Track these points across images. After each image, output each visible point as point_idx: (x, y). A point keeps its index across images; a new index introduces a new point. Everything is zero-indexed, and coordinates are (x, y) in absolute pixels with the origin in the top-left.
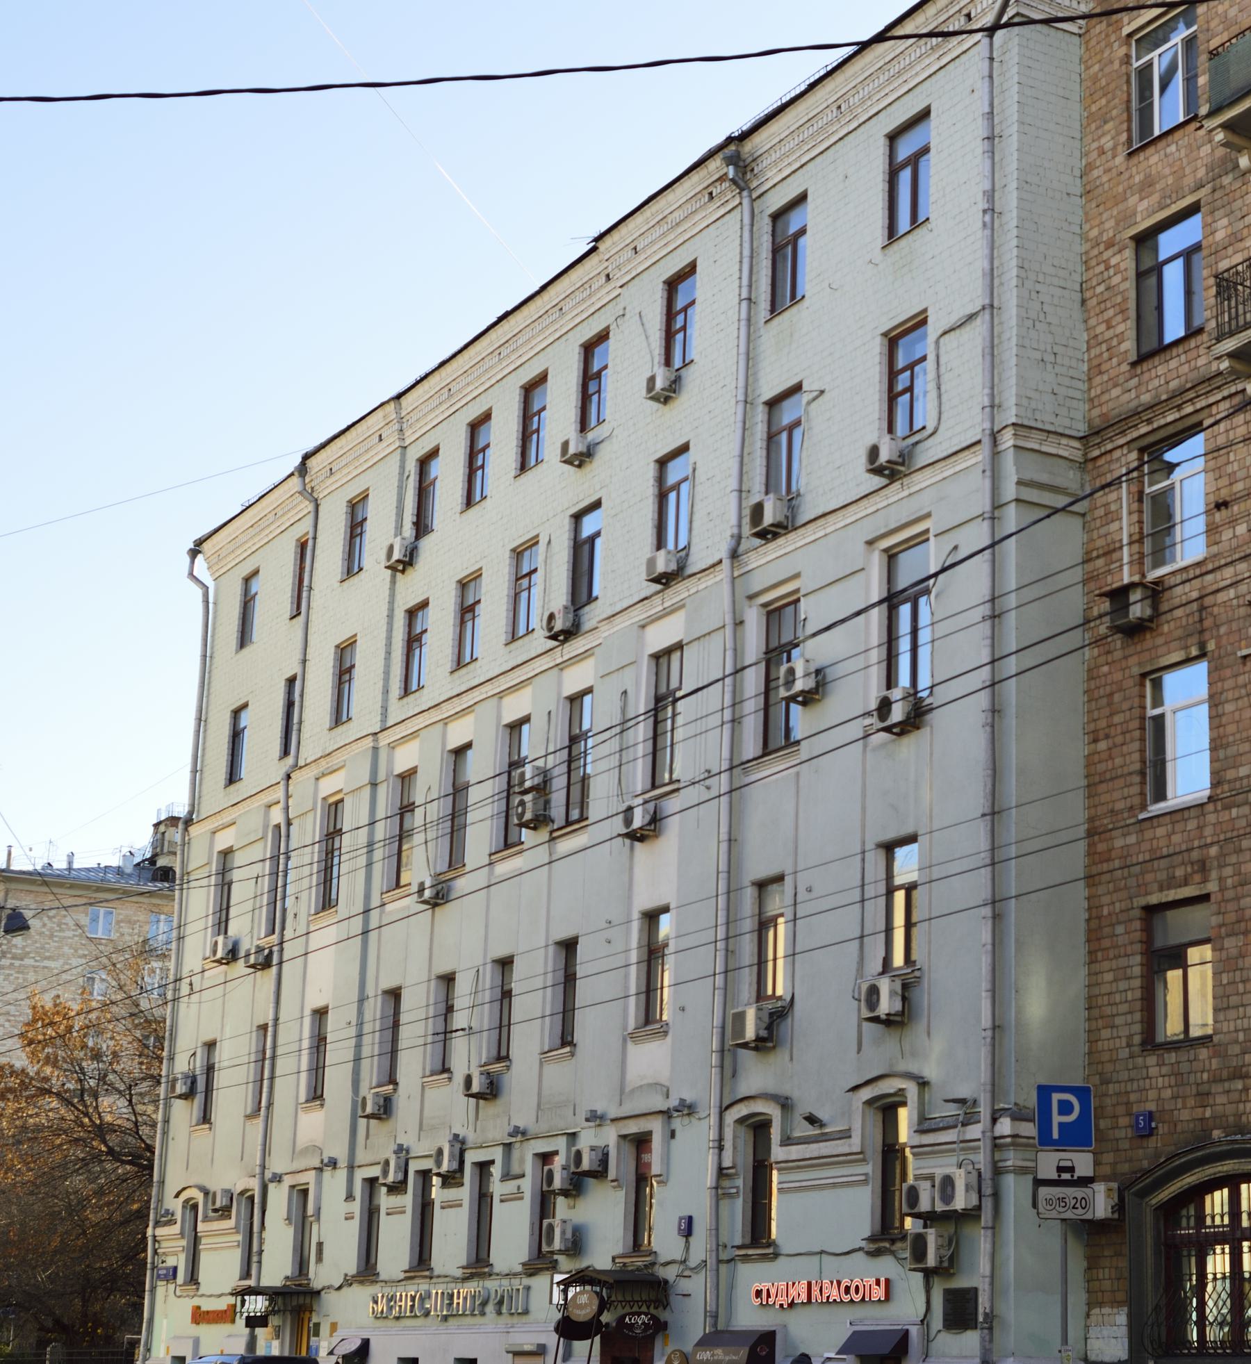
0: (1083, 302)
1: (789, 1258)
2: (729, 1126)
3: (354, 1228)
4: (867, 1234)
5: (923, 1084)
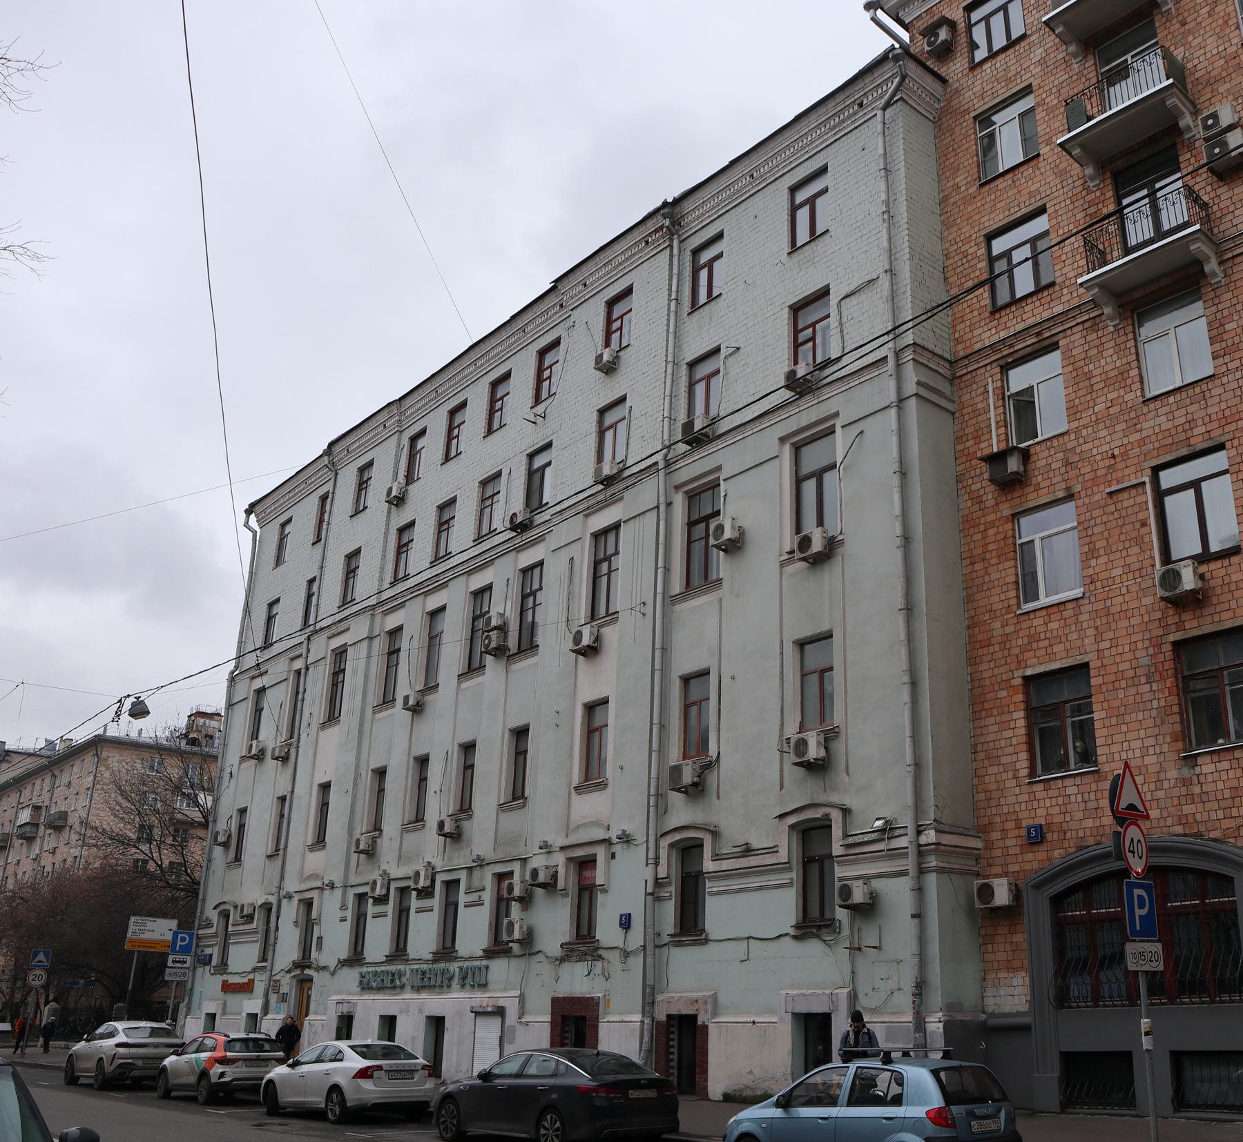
0: (946, 279)
1: (718, 943)
2: (664, 848)
3: (347, 927)
4: (794, 923)
5: (846, 811)
